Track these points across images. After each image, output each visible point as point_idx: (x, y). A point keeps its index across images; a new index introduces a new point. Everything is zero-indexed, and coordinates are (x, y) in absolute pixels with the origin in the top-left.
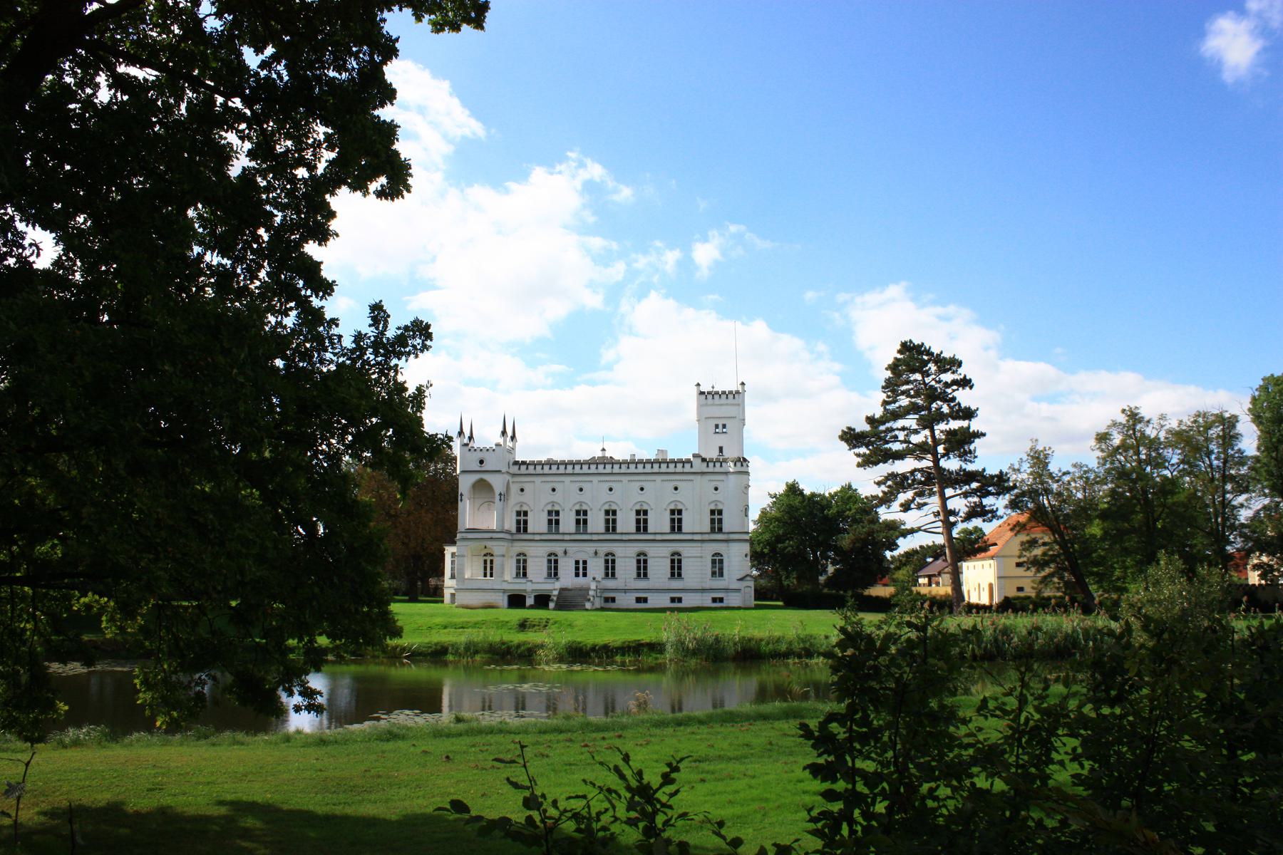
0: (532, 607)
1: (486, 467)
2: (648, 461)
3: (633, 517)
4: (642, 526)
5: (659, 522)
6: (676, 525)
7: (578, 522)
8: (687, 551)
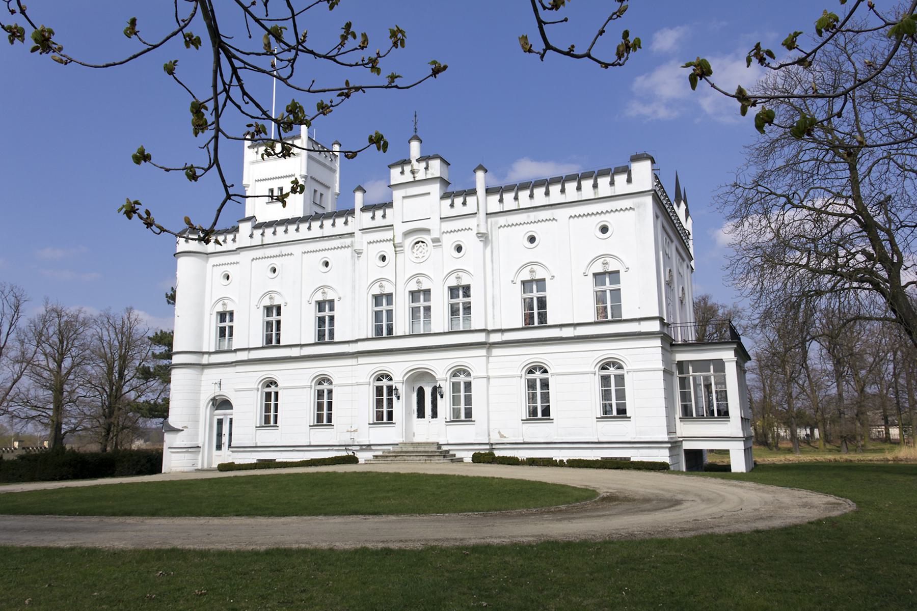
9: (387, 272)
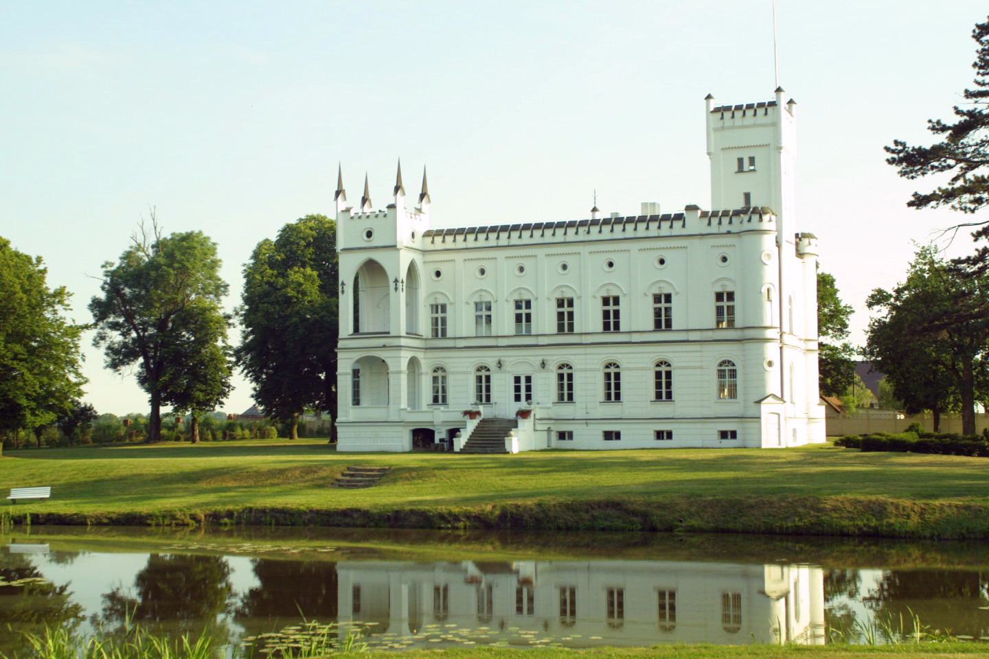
0: (462, 452)
1: (376, 241)
2: (630, 220)
3: (599, 308)
4: (611, 321)
5: (637, 315)
6: (662, 321)
7: (518, 318)
8: (679, 358)
9: (486, 283)
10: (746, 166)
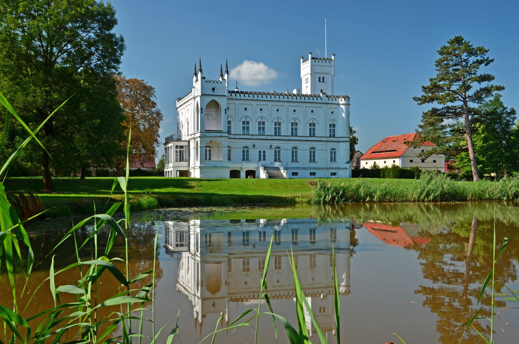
4: (294, 132)
10: (321, 80)
